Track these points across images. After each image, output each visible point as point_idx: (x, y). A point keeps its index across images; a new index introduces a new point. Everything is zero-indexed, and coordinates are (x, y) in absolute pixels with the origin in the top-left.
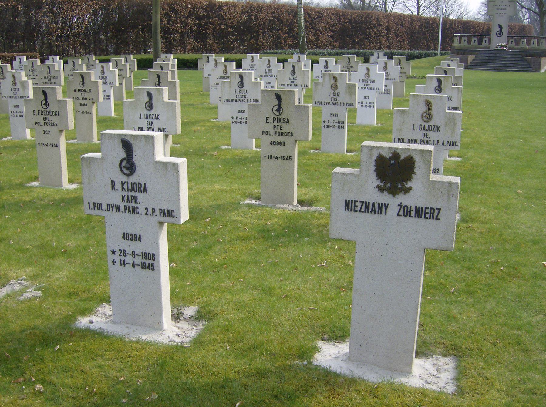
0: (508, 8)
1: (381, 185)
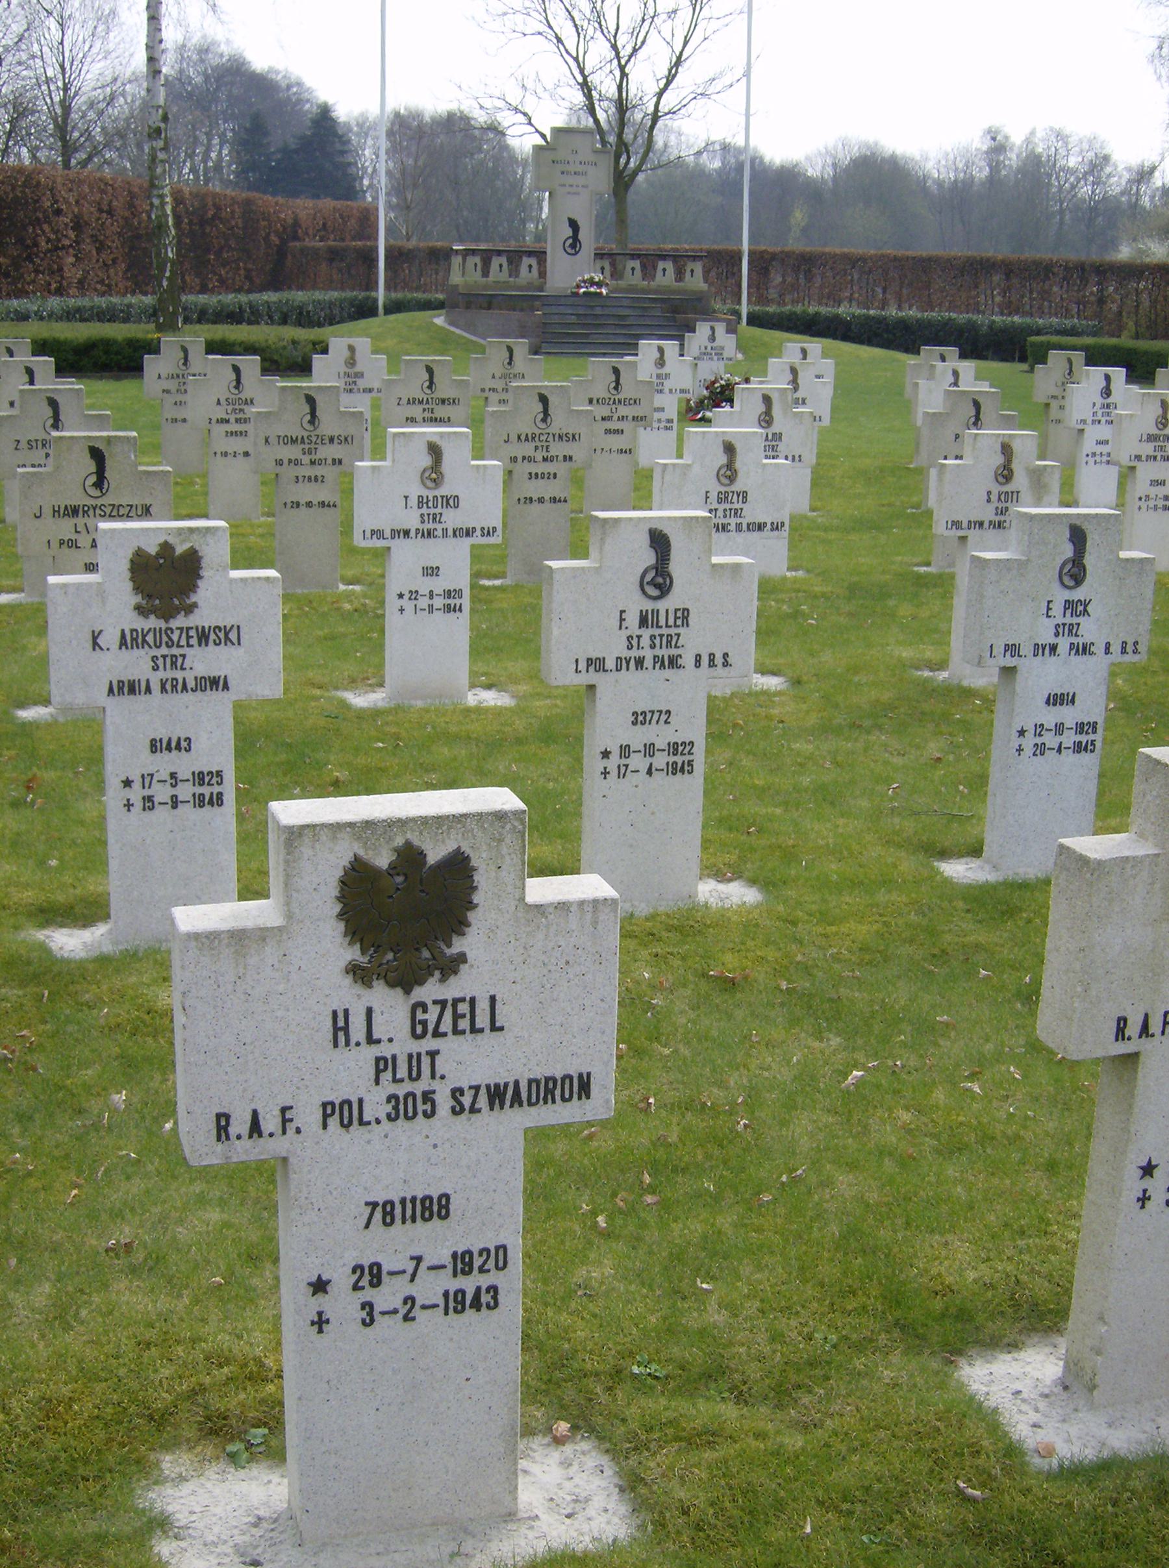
0: (591, 170)
1: (363, 960)
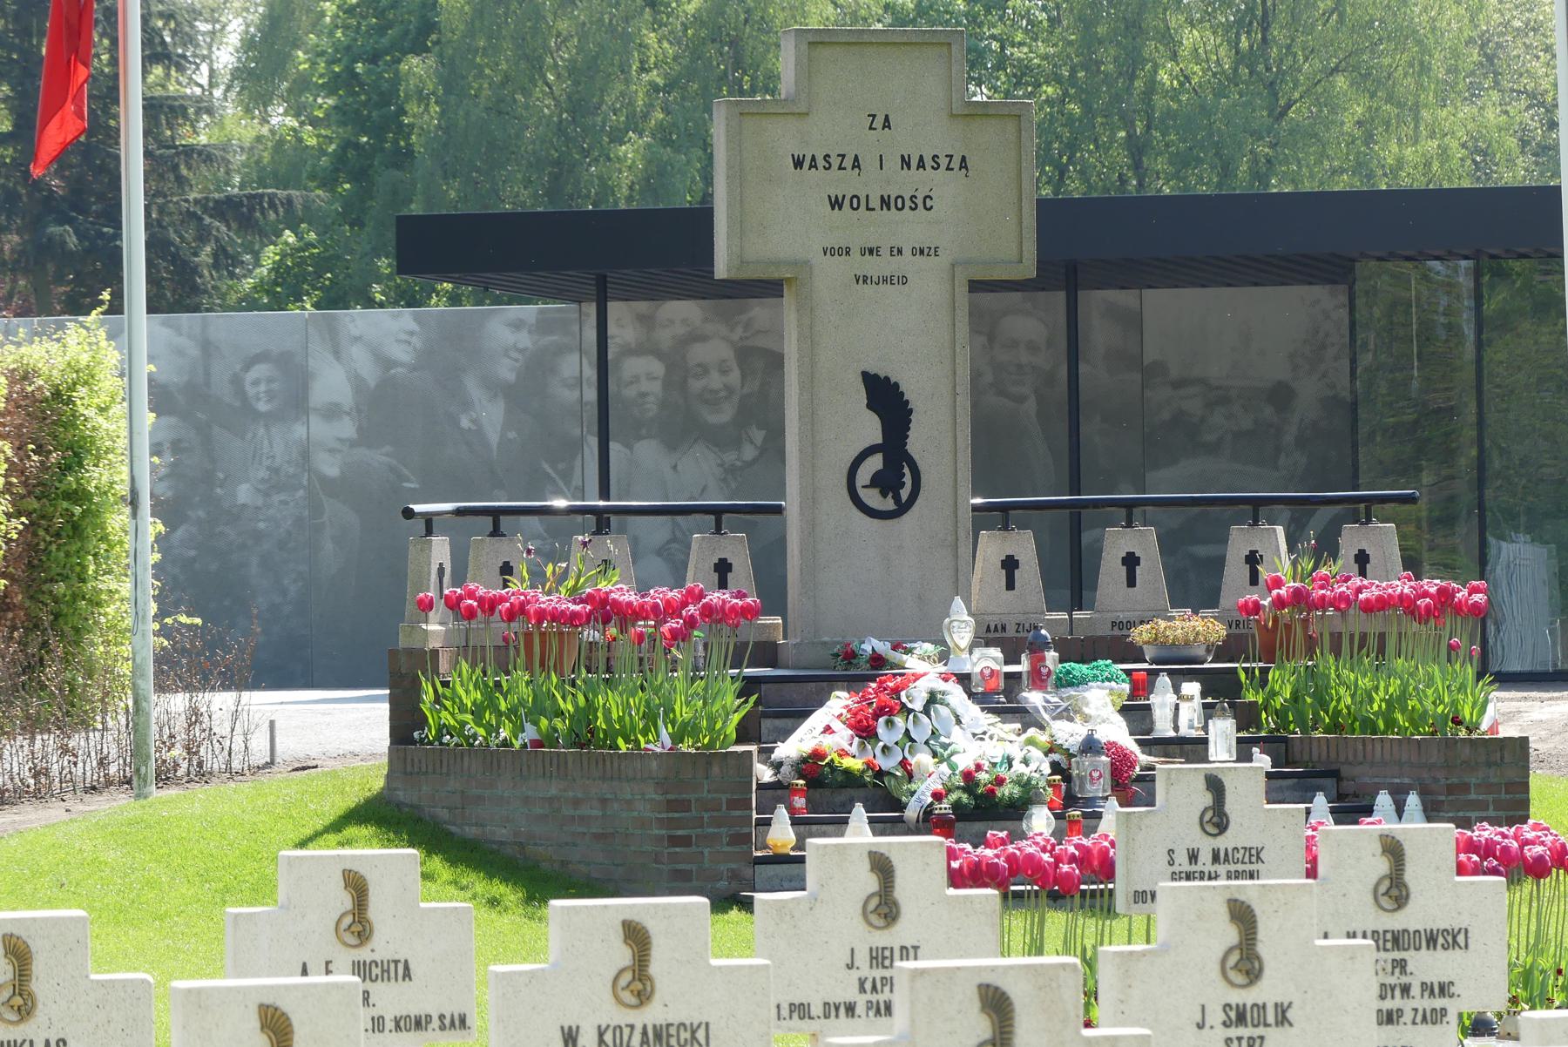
0: (944, 186)
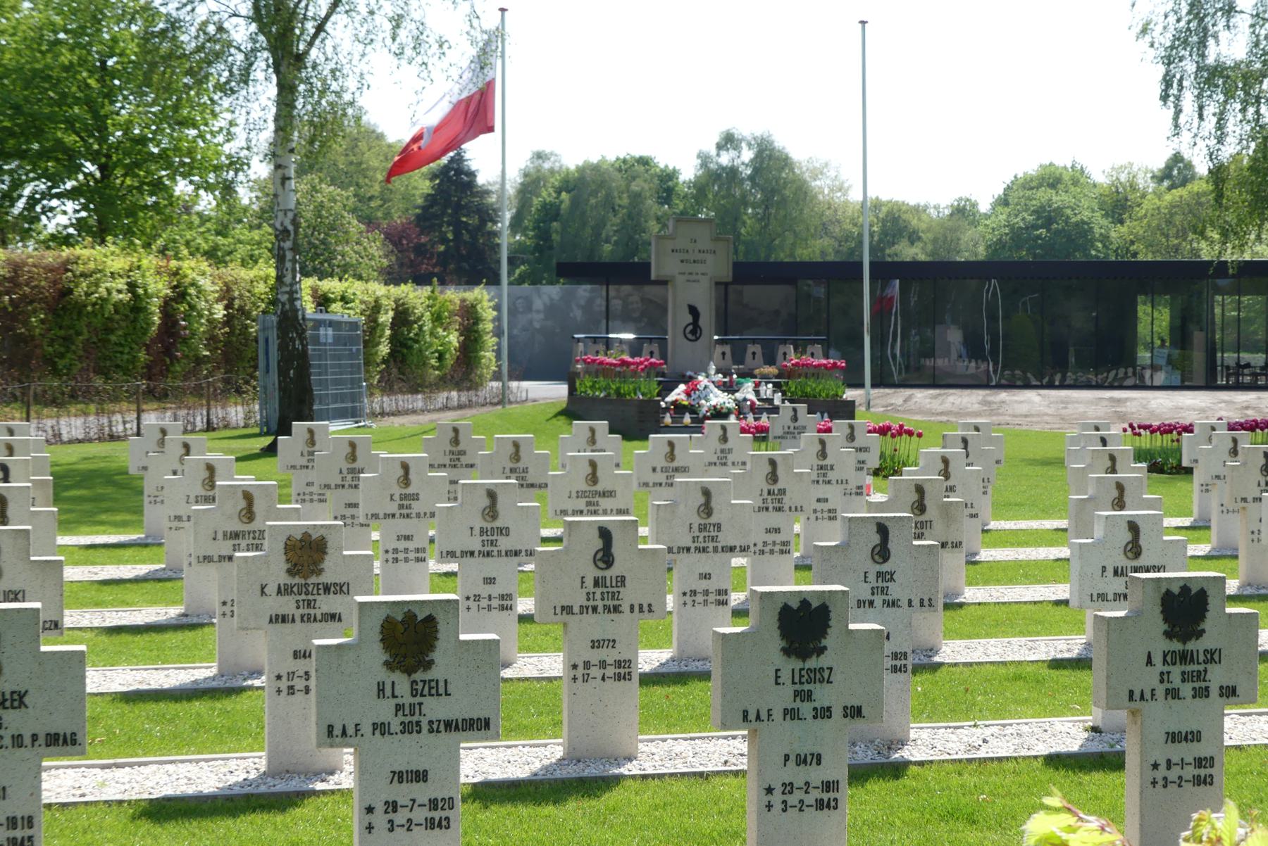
0: (709, 258)
